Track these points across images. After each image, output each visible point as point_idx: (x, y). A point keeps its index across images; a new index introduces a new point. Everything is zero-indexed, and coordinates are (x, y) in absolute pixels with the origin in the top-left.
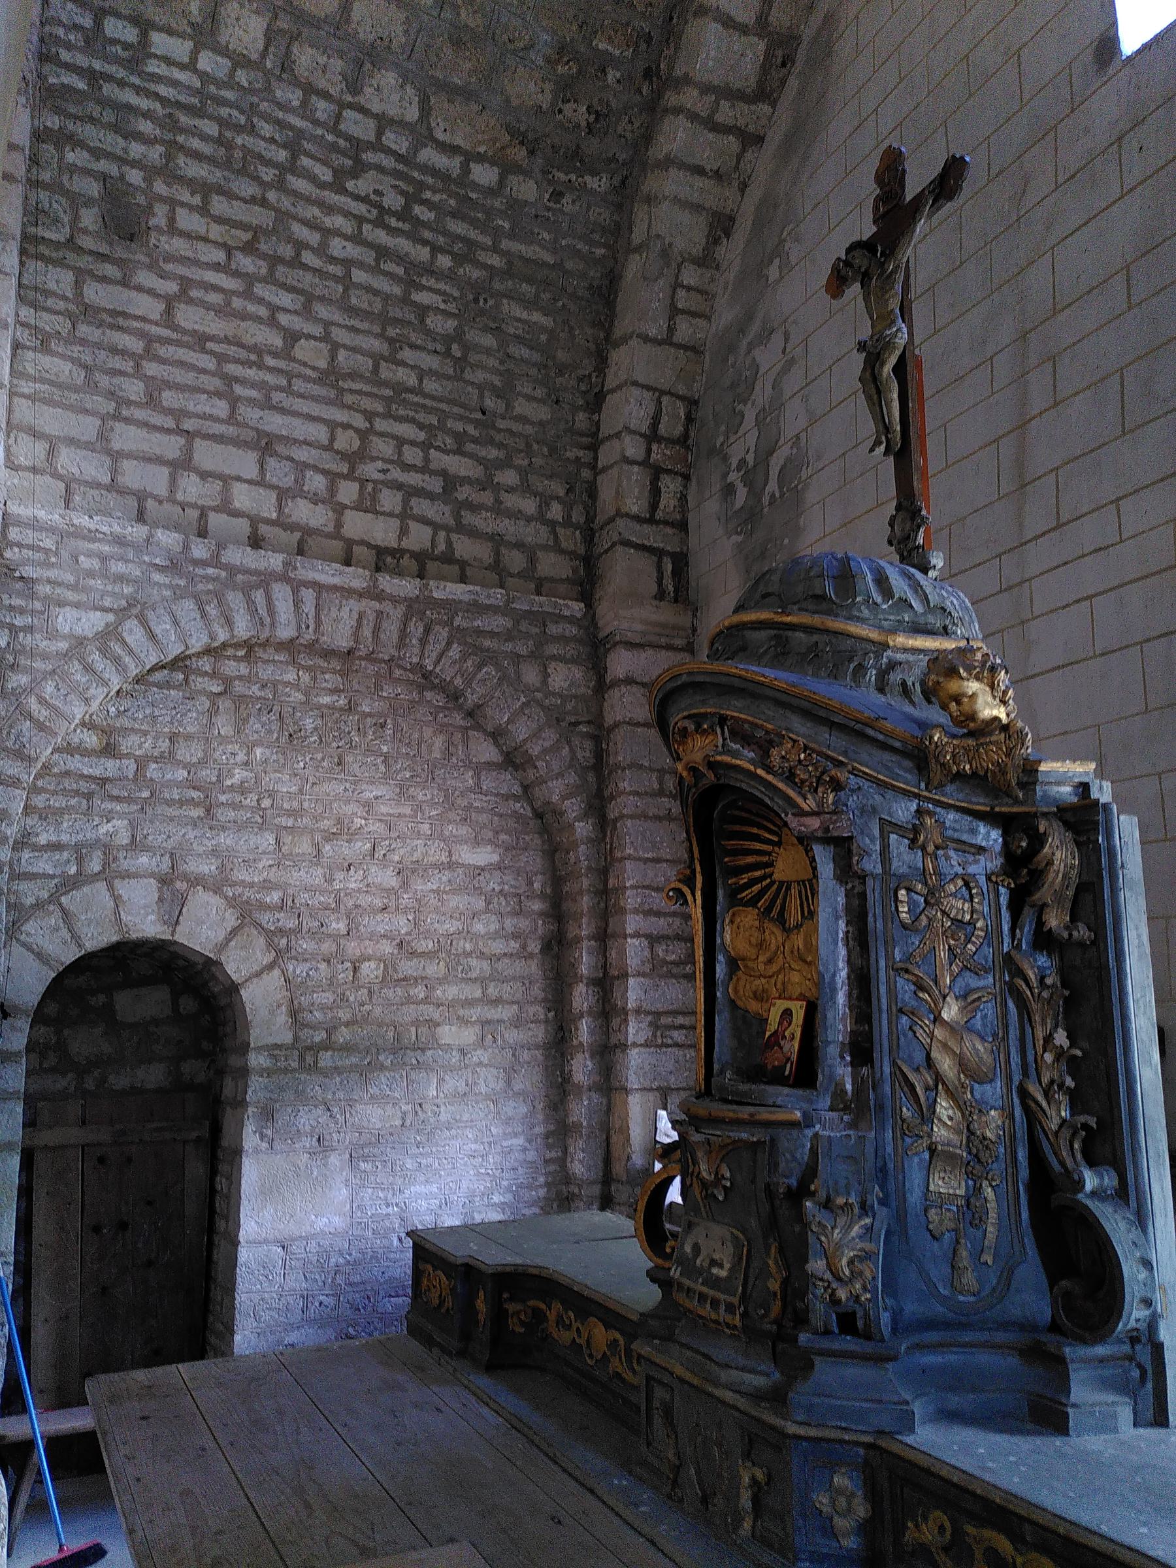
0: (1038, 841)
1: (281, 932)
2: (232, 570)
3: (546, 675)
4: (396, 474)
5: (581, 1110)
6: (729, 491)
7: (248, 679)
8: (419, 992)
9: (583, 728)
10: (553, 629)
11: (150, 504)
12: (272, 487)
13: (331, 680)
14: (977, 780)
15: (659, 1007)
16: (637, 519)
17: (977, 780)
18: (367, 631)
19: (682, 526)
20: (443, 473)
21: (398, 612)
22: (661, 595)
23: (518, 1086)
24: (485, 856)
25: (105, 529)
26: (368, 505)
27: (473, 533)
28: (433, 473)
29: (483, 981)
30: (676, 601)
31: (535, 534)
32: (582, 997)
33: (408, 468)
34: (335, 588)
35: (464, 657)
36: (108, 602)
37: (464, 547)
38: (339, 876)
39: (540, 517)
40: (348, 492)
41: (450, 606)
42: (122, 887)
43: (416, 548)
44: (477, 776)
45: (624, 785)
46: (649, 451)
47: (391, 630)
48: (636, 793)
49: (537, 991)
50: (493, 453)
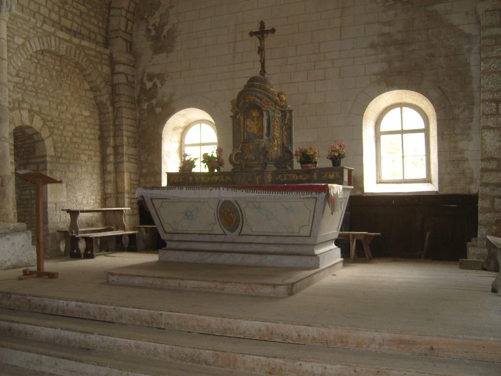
0: (286, 114)
1: (51, 127)
2: (44, 31)
3: (102, 68)
4: (71, 9)
5: (110, 177)
6: (149, 30)
7: (43, 60)
8: (77, 146)
9: (109, 83)
10: (104, 56)
11: (24, 9)
12: (48, 8)
13: (58, 63)
14: (280, 106)
15: (129, 153)
16: (123, 31)
17: (280, 106)
18: (68, 51)
19: (131, 35)
20: (80, 10)
21: (74, 47)
22: (127, 51)
23: (95, 171)
24: (87, 113)
25: (21, 16)
26: (66, 17)
27: (85, 27)
28: (78, 10)
29: (88, 145)
30: (130, 53)
31: (96, 29)
32: (110, 151)
33: (74, 8)
34: (63, 39)
35: (87, 61)
36: (23, 36)
37: (84, 32)
38: (61, 114)
39: (97, 26)
40: (62, 12)
41: (84, 47)
42: (22, 112)
43: (74, 30)
44: (85, 92)
45: (122, 99)
46: (127, 14)
47: (73, 52)
48: (124, 101)
49: (98, 149)
50: (90, 7)
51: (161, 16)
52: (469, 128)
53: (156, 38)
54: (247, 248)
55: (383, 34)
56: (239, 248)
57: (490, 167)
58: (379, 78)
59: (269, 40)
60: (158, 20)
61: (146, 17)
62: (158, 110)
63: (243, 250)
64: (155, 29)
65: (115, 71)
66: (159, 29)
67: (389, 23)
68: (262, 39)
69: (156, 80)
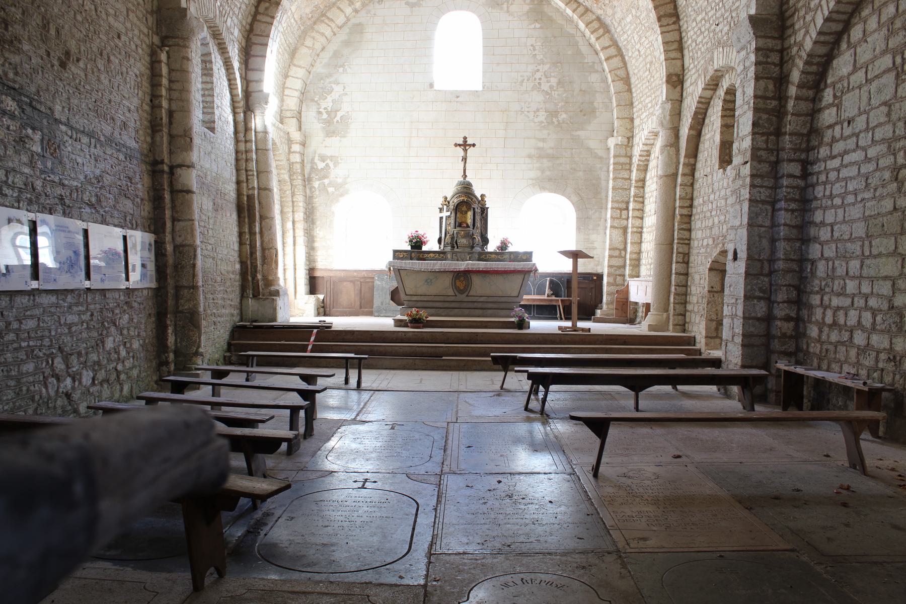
6: (320, 113)
51: (334, 101)
52: (599, 225)
53: (329, 122)
54: (470, 305)
55: (539, 148)
56: (465, 305)
57: (614, 255)
58: (534, 182)
59: (471, 151)
60: (330, 104)
61: (316, 99)
62: (331, 190)
63: (468, 307)
64: (327, 112)
65: (292, 150)
66: (332, 113)
67: (543, 140)
68: (465, 151)
69: (328, 161)
